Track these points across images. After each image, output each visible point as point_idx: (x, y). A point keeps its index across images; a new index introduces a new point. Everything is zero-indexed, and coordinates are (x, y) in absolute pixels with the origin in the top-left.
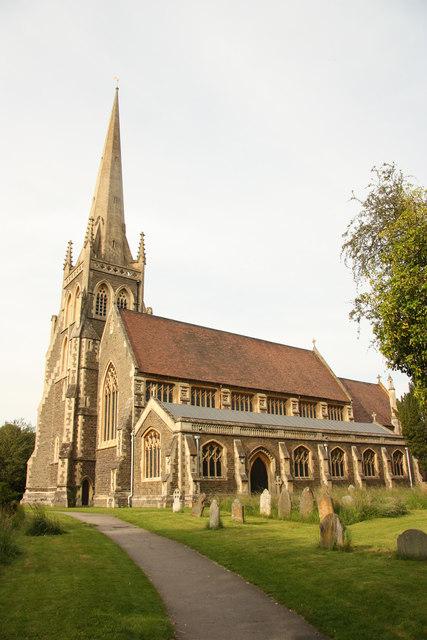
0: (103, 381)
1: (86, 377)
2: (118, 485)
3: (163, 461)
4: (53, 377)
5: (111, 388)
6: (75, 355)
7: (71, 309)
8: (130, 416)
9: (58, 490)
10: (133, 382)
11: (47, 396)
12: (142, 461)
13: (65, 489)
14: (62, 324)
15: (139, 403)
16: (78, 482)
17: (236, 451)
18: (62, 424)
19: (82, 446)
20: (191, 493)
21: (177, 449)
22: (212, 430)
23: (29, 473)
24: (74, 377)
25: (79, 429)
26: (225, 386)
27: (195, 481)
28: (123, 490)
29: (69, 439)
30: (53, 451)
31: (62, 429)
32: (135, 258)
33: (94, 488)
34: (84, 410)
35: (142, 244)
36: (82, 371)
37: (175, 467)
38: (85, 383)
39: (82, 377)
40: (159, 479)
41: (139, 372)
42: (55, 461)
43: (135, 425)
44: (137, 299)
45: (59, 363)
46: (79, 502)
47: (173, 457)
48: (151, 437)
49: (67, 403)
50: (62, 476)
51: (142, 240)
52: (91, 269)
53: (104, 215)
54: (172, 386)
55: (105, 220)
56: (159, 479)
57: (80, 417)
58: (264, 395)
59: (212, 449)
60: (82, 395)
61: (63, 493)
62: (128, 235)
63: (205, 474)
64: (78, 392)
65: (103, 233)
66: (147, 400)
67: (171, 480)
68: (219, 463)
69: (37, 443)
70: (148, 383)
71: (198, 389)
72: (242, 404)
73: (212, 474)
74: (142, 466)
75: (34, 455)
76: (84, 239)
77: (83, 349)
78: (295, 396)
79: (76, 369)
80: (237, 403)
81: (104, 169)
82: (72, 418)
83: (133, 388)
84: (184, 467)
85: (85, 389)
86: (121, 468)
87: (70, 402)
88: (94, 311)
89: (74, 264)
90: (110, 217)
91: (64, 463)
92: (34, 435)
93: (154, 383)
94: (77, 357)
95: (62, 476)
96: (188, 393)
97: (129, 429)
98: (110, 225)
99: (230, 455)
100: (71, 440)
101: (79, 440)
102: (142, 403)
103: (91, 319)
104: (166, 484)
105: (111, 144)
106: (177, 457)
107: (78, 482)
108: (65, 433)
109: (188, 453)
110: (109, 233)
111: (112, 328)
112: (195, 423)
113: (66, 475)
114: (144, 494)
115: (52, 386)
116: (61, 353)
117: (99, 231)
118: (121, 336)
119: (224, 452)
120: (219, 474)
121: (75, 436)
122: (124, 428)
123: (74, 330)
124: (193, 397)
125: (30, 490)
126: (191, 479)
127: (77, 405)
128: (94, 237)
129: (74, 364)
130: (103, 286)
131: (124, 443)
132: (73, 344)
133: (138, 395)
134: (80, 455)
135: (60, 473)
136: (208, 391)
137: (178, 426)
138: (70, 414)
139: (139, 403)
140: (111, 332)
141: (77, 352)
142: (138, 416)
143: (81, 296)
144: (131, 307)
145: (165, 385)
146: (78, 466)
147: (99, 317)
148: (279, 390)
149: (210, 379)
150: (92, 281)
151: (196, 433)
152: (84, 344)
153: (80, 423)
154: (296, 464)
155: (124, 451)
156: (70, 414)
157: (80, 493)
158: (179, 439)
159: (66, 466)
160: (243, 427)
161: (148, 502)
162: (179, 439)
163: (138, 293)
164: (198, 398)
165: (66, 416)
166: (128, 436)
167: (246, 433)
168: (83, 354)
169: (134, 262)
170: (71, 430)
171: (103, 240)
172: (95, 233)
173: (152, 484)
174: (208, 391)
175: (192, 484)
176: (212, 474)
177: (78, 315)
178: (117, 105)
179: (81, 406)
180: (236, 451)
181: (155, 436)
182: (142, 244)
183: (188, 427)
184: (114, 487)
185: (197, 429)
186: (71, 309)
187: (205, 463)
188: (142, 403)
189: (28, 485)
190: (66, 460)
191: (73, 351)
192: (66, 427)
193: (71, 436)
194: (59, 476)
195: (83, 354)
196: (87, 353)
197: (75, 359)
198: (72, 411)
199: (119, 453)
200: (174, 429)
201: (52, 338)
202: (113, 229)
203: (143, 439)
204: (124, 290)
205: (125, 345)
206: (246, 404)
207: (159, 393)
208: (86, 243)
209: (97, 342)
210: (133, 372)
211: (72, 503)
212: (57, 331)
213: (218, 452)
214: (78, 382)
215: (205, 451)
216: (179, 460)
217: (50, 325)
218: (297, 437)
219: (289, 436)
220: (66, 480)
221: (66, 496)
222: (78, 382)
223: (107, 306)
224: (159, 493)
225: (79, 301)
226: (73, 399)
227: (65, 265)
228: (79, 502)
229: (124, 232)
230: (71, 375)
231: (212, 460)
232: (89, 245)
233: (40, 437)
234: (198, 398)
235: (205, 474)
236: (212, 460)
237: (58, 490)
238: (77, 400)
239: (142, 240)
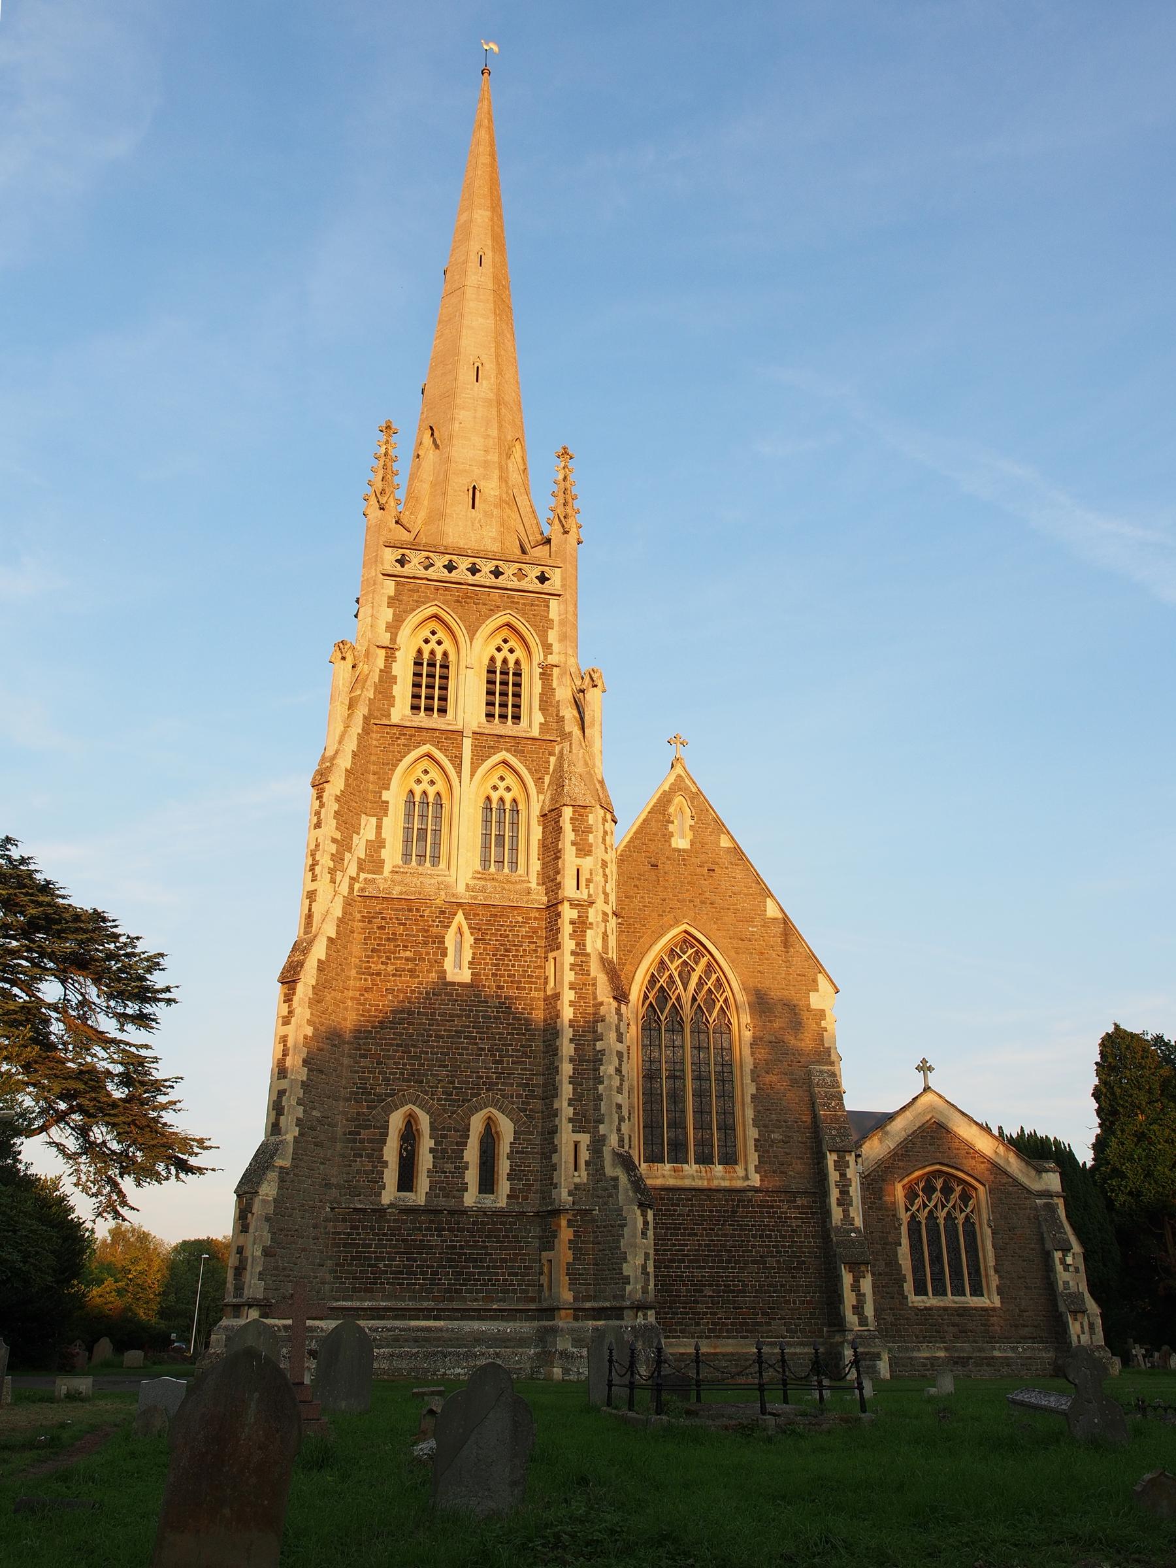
68: (971, 1235)
213: (965, 1198)
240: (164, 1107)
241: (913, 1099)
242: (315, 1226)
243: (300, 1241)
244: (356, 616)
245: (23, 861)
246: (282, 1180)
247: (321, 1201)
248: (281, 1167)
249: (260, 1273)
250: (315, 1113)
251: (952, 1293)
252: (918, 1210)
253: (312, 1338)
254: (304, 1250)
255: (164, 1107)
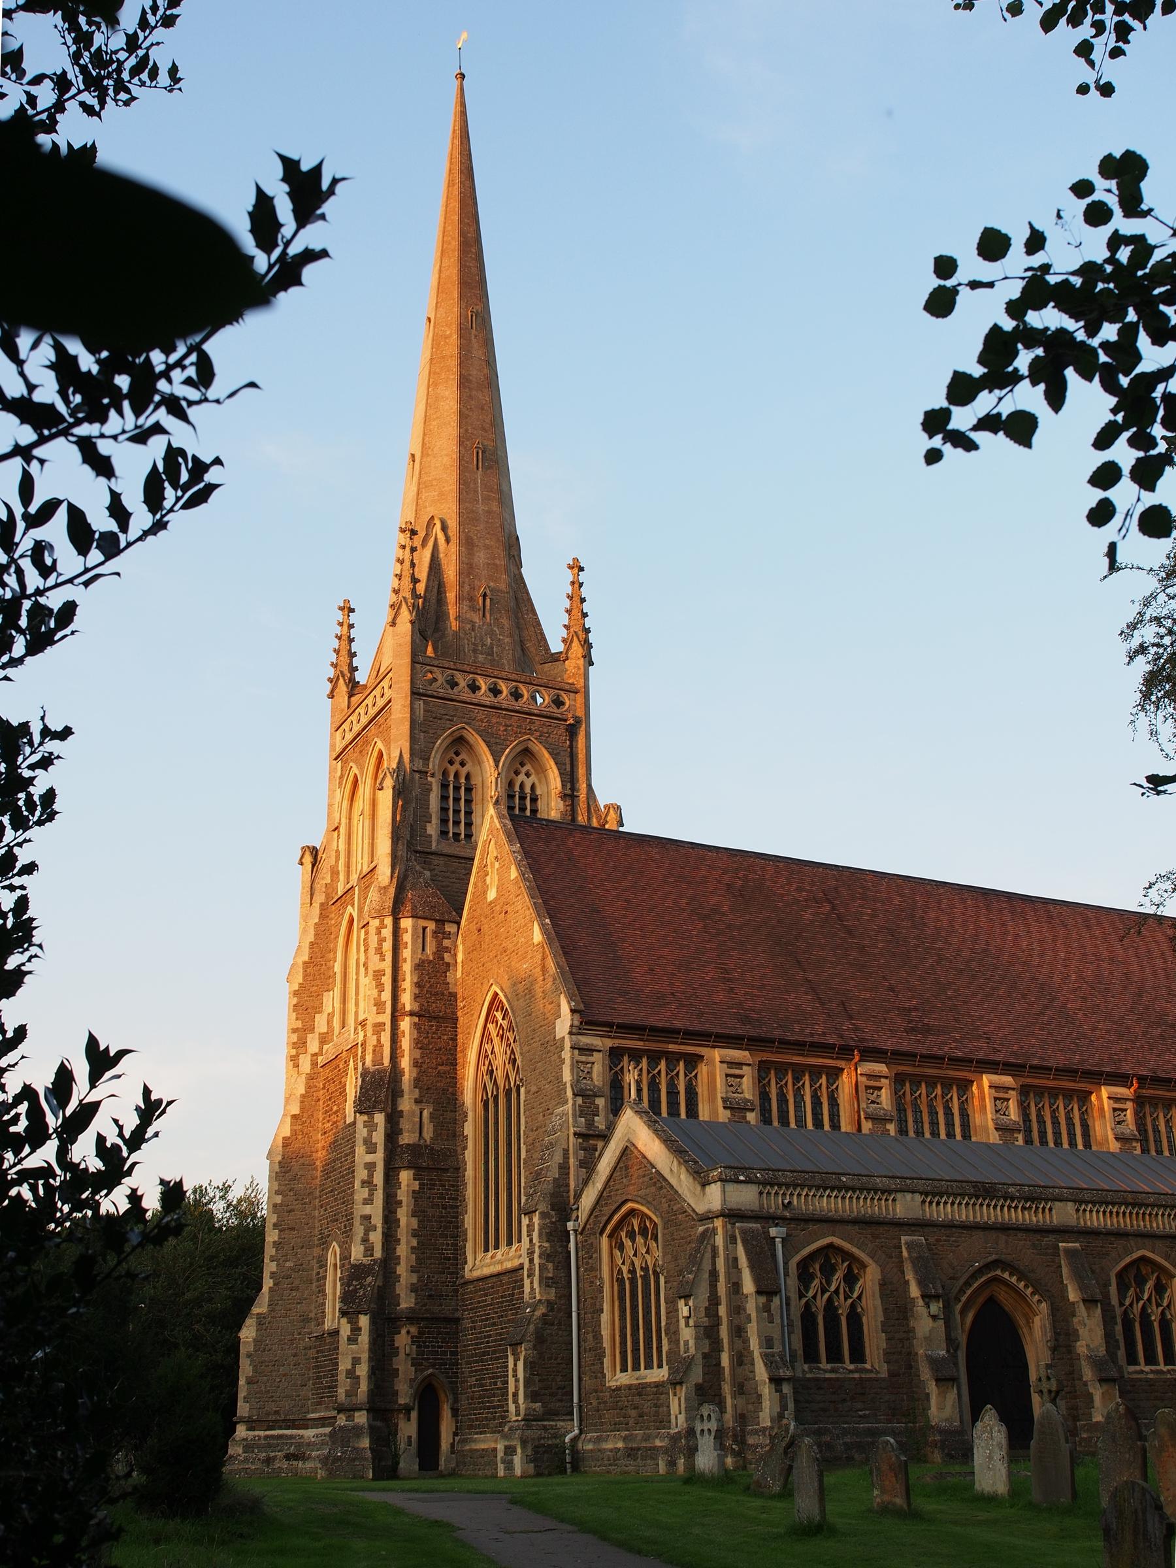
0: (472, 1055)
1: (417, 1044)
2: (532, 1396)
3: (673, 1312)
4: (313, 1046)
5: (499, 1074)
6: (379, 974)
7: (361, 827)
8: (564, 1168)
9: (342, 1420)
10: (567, 1054)
11: (295, 1110)
12: (605, 1317)
13: (361, 1418)
14: (335, 873)
15: (590, 1124)
16: (404, 1393)
17: (910, 1276)
18: (348, 1201)
19: (413, 1270)
20: (765, 1420)
21: (714, 1274)
22: (826, 1204)
23: (246, 1368)
24: (379, 1045)
25: (403, 1215)
26: (871, 1053)
27: (776, 1381)
28: (550, 1414)
29: (369, 1250)
30: (322, 1291)
31: (349, 1217)
32: (556, 646)
33: (455, 1412)
34: (415, 1149)
35: (577, 599)
36: (405, 1024)
37: (709, 1332)
38: (416, 1064)
39: (406, 1043)
40: (659, 1374)
41: (586, 1021)
42: (328, 1325)
43: (578, 1196)
44: (570, 778)
45: (331, 1001)
46: (408, 1462)
47: (703, 1292)
48: (632, 1235)
49: (362, 1132)
50: (351, 1374)
51: (577, 584)
52: (415, 694)
53: (449, 510)
54: (693, 1061)
55: (453, 525)
56: (659, 1374)
57: (405, 1176)
58: (1007, 1080)
59: (828, 1271)
60: (406, 1104)
61: (357, 1431)
62: (528, 573)
63: (811, 1356)
64: (395, 1092)
65: (450, 572)
66: (616, 1110)
67: (697, 1375)
68: (855, 1318)
69: (270, 1267)
70: (615, 1055)
71: (781, 1069)
72: (933, 1113)
73: (834, 1356)
74: (605, 1332)
75: (261, 1307)
76: (389, 598)
77: (407, 953)
78: (1121, 1079)
79: (386, 1018)
80: (917, 1111)
81: (434, 360)
82: (379, 1178)
83: (567, 1076)
84: (739, 1332)
85: (417, 1083)
86: (540, 1340)
87: (371, 1126)
88: (432, 829)
89: (361, 677)
90: (467, 516)
91: (356, 1330)
92: (259, 1232)
93: (635, 1055)
94: (387, 980)
95: (351, 1374)
96: (1129, 1114)
97: (561, 1207)
98: (468, 544)
99: (892, 1290)
100: (378, 1254)
101: (402, 1250)
102: (600, 1122)
103: (425, 856)
104: (683, 1391)
105: (454, 272)
106: (714, 1301)
107: (404, 1393)
108: (359, 1230)
109: (748, 1286)
110: (467, 570)
111: (492, 880)
112: (768, 1182)
113: (363, 1370)
114: (616, 1427)
115: (311, 1078)
116: (337, 968)
117: (435, 566)
118: (523, 906)
119: (871, 1277)
120: (858, 1355)
121: (390, 1239)
122: (543, 1207)
123: (373, 895)
124: (764, 1096)
125: (252, 1425)
126: (761, 1372)
127: (392, 1134)
128: (421, 588)
129: (379, 1005)
130: (459, 742)
131: (546, 1256)
132: (373, 940)
133: (585, 1094)
134: (406, 1301)
135: (344, 1365)
136: (815, 1072)
137: (713, 1197)
138: (371, 1167)
139: (590, 1124)
140: (492, 895)
141: (387, 965)
142: (589, 1165)
143: (389, 783)
144: (553, 808)
145: (673, 1059)
146: (403, 1340)
147: (422, 923)
148: (1061, 1061)
149: (819, 1031)
150: (420, 730)
151: (773, 1219)
152: (407, 938)
153: (403, 1195)
154: (1128, 1325)
155: (546, 1282)
156: (371, 1167)
157: (408, 1429)
158: (719, 1240)
159: (364, 1338)
160: (933, 1192)
161: (631, 1453)
162: (719, 1240)
163: (573, 756)
164: (782, 1099)
165: (361, 1174)
166: (556, 1234)
167: (944, 1212)
168: (407, 968)
169: (556, 658)
170: (377, 1220)
171: (451, 596)
172: (423, 573)
173: (640, 1389)
174: (815, 1072)
175: (766, 1390)
176: (834, 1356)
177: (384, 846)
178: (462, 103)
179: (406, 1138)
180: (910, 1276)
181: (644, 1231)
182: (577, 599)
183: (745, 1196)
184: (517, 1404)
185: (774, 1203)
186: (361, 827)
187: (808, 1317)
188: (600, 1122)
189: (243, 1409)
190: (364, 1321)
191: (375, 963)
192: (362, 1210)
193: (376, 1237)
194: (341, 1377)
195: (407, 968)
196: (419, 967)
197: (380, 987)
198: (379, 1157)
199: (532, 1288)
200: (701, 1209)
201: (305, 918)
202: (481, 557)
203: (605, 1241)
204: (526, 754)
205: (537, 936)
206: (1056, 1122)
207: (654, 1086)
208: (395, 608)
209: (450, 928)
210: (564, 1023)
211: (386, 1469)
212: (320, 898)
213: (851, 1279)
214: (394, 1057)
215: (805, 1277)
216: (722, 1310)
217: (298, 876)
218: (1126, 1223)
219: (1095, 1219)
220: (364, 1387)
221: (365, 1443)
222: (394, 1057)
223: (477, 809)
224: (663, 1421)
225: (386, 798)
226: (380, 1118)
227: (334, 681)
228: (408, 1462)
229: (519, 565)
230: (372, 1041)
231: (830, 1307)
232: (405, 616)
233: (276, 1244)
234: (782, 1099)
235: (811, 1356)
236: (830, 1307)
237: (342, 1420)
238: (393, 1119)
239: (577, 584)
240: (207, 1204)
241: (590, 646)
242: (295, 1355)
243: (282, 1369)
244: (118, 574)
245: (1143, 684)
246: (260, 1324)
247: (300, 1334)
248: (258, 1314)
249: (245, 1398)
250: (288, 1264)
251: (827, 1359)
252: (814, 1297)
253: (291, 1444)
254: (284, 1375)
255: (207, 1204)
